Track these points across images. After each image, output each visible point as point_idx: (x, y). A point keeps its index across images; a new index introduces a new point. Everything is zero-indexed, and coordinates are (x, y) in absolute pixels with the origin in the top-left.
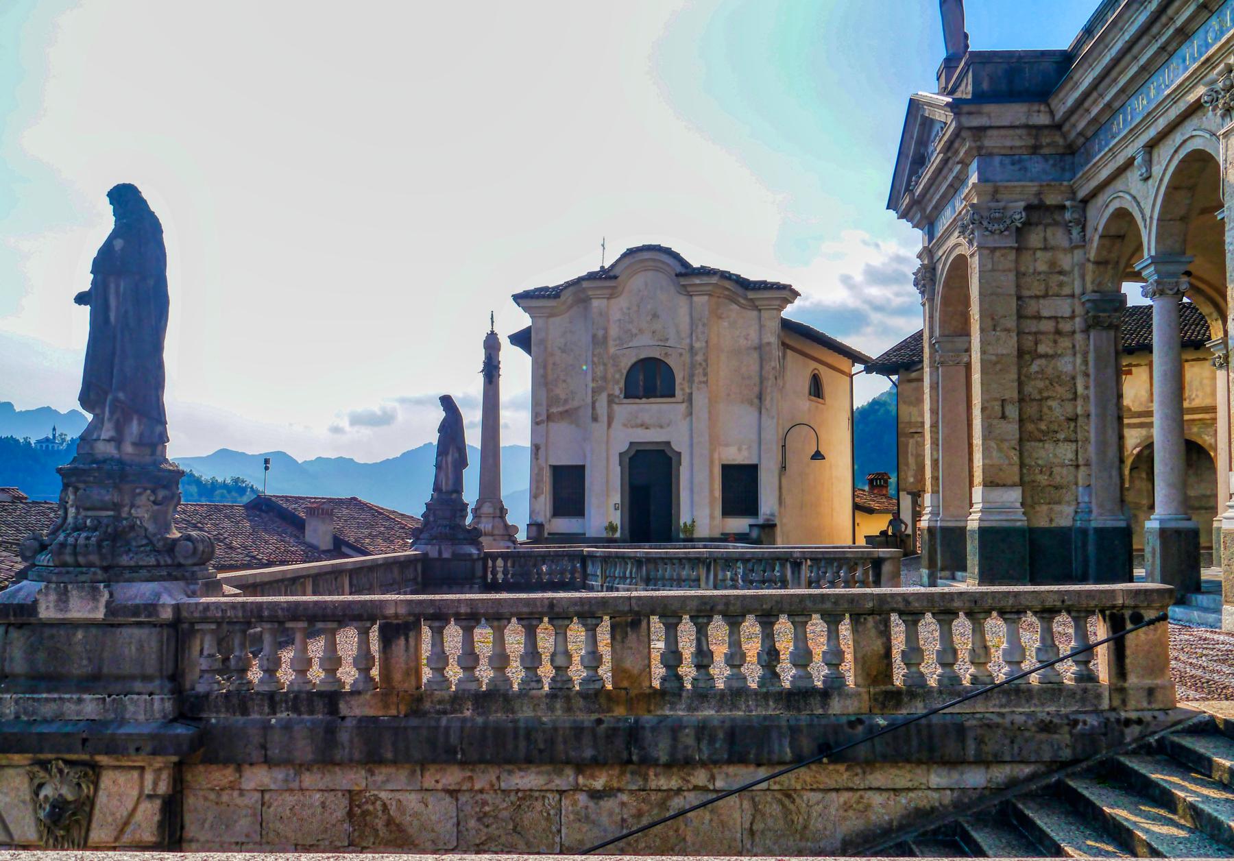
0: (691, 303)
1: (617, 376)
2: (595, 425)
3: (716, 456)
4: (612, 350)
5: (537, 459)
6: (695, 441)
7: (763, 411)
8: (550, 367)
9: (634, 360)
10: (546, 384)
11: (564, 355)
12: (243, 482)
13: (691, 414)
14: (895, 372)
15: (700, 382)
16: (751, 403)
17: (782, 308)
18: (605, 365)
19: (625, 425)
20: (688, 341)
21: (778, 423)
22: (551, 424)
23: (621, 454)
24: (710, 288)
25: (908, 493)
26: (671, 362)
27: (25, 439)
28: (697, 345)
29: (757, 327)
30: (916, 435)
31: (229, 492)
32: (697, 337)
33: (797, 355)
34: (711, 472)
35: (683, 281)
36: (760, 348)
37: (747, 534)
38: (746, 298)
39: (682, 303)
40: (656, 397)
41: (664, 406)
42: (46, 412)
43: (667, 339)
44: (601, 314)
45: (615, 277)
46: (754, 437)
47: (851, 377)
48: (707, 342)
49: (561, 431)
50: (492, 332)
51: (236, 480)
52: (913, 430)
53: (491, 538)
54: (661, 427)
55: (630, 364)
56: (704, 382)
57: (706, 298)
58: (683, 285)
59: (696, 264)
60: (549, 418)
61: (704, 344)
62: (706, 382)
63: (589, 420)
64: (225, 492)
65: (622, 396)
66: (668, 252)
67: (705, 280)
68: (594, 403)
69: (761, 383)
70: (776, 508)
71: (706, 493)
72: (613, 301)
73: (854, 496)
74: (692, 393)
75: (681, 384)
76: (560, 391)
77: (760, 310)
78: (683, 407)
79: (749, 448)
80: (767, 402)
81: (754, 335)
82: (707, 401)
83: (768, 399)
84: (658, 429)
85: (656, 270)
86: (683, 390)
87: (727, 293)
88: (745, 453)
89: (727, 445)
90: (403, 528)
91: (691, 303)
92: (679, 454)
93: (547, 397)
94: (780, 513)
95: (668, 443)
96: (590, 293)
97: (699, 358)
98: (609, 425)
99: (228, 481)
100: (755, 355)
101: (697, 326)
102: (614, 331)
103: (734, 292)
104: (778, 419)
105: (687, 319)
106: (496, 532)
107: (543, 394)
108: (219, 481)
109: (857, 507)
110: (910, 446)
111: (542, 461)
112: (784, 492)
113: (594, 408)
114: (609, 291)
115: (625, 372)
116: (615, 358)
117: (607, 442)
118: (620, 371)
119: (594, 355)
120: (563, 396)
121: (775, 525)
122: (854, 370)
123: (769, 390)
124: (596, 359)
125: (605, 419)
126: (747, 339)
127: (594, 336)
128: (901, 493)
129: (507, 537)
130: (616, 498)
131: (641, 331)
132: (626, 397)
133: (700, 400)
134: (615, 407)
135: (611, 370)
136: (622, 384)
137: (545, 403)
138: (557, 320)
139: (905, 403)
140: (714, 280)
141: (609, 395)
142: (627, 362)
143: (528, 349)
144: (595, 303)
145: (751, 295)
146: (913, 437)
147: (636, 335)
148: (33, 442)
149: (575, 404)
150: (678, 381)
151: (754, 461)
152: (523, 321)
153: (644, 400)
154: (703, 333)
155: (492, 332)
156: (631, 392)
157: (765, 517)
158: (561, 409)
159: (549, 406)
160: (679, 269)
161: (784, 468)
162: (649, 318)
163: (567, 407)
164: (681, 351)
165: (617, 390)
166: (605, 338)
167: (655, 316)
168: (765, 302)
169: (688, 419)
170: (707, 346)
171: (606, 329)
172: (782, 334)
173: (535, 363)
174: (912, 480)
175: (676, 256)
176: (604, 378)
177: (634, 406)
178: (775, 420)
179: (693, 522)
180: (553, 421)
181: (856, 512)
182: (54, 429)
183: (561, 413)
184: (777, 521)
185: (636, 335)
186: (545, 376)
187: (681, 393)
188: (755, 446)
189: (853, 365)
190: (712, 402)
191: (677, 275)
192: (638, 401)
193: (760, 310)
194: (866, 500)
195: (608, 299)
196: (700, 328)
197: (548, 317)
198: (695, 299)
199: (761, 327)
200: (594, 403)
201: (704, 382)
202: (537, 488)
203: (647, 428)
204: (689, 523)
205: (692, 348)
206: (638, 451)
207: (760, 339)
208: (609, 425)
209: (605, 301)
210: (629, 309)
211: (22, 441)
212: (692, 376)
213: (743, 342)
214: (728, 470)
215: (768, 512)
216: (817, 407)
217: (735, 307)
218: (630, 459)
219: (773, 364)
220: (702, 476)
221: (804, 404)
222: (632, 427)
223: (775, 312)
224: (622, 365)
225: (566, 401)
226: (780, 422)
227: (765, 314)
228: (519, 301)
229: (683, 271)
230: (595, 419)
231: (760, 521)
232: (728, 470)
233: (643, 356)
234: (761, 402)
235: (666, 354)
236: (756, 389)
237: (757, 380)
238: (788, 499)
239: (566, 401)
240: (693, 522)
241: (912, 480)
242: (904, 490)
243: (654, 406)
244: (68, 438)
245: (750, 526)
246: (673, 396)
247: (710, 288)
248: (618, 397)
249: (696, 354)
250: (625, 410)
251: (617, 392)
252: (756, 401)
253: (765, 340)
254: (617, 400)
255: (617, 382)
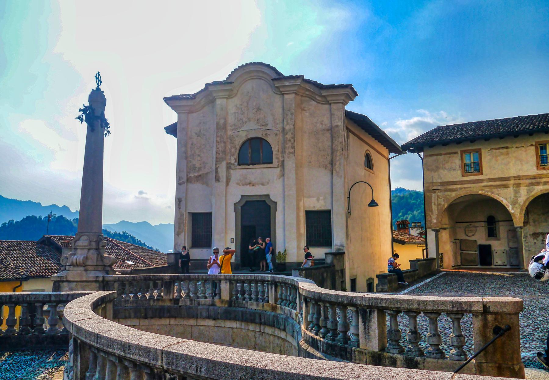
0: (283, 99)
1: (233, 150)
2: (217, 184)
3: (301, 204)
4: (230, 133)
5: (180, 208)
6: (286, 193)
7: (334, 173)
8: (189, 145)
9: (244, 139)
10: (186, 158)
11: (199, 138)
12: (127, 233)
13: (283, 175)
14: (422, 151)
15: (290, 153)
16: (326, 167)
17: (345, 103)
18: (225, 143)
19: (238, 184)
20: (281, 125)
21: (344, 182)
22: (190, 185)
23: (235, 204)
24: (295, 88)
25: (433, 230)
26: (269, 139)
27: (40, 216)
28: (287, 127)
29: (328, 115)
30: (437, 191)
31: (120, 237)
32: (287, 122)
33: (355, 138)
34: (298, 216)
35: (277, 84)
36: (331, 130)
37: (324, 260)
38: (321, 96)
39: (277, 101)
40: (259, 163)
41: (265, 170)
42: (65, 208)
43: (267, 125)
44: (222, 109)
45: (231, 83)
46: (329, 190)
47: (389, 160)
48: (294, 125)
49: (196, 188)
50: (98, 89)
51: (124, 233)
52: (435, 188)
53: (82, 269)
54: (263, 184)
55: (241, 142)
56: (292, 153)
57: (293, 95)
58: (277, 87)
59: (286, 74)
60: (189, 180)
61: (292, 127)
62: (293, 153)
63: (214, 180)
64: (119, 237)
65: (236, 164)
66: (268, 66)
67: (293, 82)
68: (217, 169)
69: (332, 153)
70: (344, 240)
71: (294, 230)
72: (230, 100)
73: (392, 234)
74: (284, 161)
75: (276, 154)
76: (196, 163)
77: (330, 104)
78: (278, 170)
79: (325, 199)
80: (337, 167)
81: (327, 121)
82: (294, 165)
83: (338, 164)
84: (261, 186)
85: (260, 78)
86: (278, 158)
87: (307, 93)
88: (322, 202)
89: (310, 197)
90: (128, 254)
91: (283, 99)
92: (276, 203)
93: (187, 166)
94: (347, 244)
95: (268, 196)
96: (214, 95)
97: (289, 136)
98: (227, 184)
99: (121, 233)
100: (328, 135)
101: (287, 115)
102: (231, 120)
103: (313, 92)
104: (345, 178)
105: (281, 110)
106: (89, 263)
107: (184, 163)
108: (118, 233)
109: (394, 240)
110: (433, 199)
111: (183, 210)
112: (350, 230)
113: (217, 172)
114: (227, 93)
115: (238, 147)
116: (231, 138)
117: (226, 196)
118: (235, 147)
119: (217, 137)
120: (198, 166)
121: (344, 253)
122: (390, 156)
123: (338, 158)
124: (218, 139)
125: (225, 180)
126: (322, 124)
127: (218, 124)
128: (428, 230)
129: (100, 268)
130: (232, 235)
131: (249, 119)
132: (239, 164)
133: (290, 164)
134: (232, 171)
135: (229, 146)
136: (236, 156)
137: (185, 171)
138: (195, 115)
139: (428, 170)
140: (298, 82)
141: (227, 164)
142: (239, 142)
143: (175, 135)
144: (218, 102)
145: (324, 93)
146: (435, 192)
147: (246, 122)
148: (42, 217)
149: (206, 170)
150: (274, 153)
151: (329, 208)
152: (172, 117)
153: (251, 166)
154: (291, 119)
155: (98, 89)
156: (242, 162)
157: (337, 247)
158: (196, 174)
159: (188, 172)
160: (274, 76)
161: (349, 212)
162: (254, 111)
163: (200, 173)
164: (276, 132)
165: (233, 160)
166: (225, 124)
167: (259, 109)
168: (334, 98)
169: (281, 179)
170: (294, 128)
171: (225, 119)
172: (346, 121)
173: (179, 143)
174: (435, 221)
175: (274, 69)
176: (224, 152)
177: (245, 171)
178: (343, 179)
179: (285, 251)
180: (191, 182)
181: (394, 243)
182: (51, 212)
183: (197, 177)
184: (345, 251)
185: (246, 122)
186: (186, 152)
187: (277, 160)
188: (329, 198)
189: (389, 154)
190: (298, 166)
191: (272, 80)
192: (247, 167)
193: (330, 104)
194: (397, 235)
195: (227, 98)
196: (289, 116)
197: (189, 113)
198: (286, 96)
199: (332, 115)
200: (217, 169)
201: (292, 153)
202: (179, 228)
203: (253, 186)
204: (282, 252)
205: (284, 129)
206: (247, 202)
207: (331, 123)
208: (227, 184)
209: (225, 100)
210: (241, 105)
211: (38, 217)
212: (284, 148)
213: (319, 126)
214: (309, 214)
215: (339, 244)
216: (369, 175)
217: (314, 103)
218: (242, 207)
219: (340, 140)
220: (291, 218)
221: (362, 172)
222: (243, 185)
223: (341, 105)
224: (237, 143)
225: (200, 169)
226: (346, 180)
227: (334, 106)
228: (168, 102)
229: (277, 77)
230: (218, 180)
231: (334, 250)
232: (309, 214)
233: (250, 136)
234: (332, 167)
235: (266, 134)
236: (329, 158)
237: (329, 152)
238: (352, 235)
239: (200, 169)
240: (285, 251)
241: (435, 221)
242: (430, 228)
243: (258, 170)
244: (57, 216)
245: (326, 254)
246: (271, 163)
247: (295, 88)
248: (234, 164)
249: (287, 134)
250: (238, 173)
251: (233, 161)
252: (329, 166)
253: (335, 124)
254: (232, 167)
255: (233, 155)
